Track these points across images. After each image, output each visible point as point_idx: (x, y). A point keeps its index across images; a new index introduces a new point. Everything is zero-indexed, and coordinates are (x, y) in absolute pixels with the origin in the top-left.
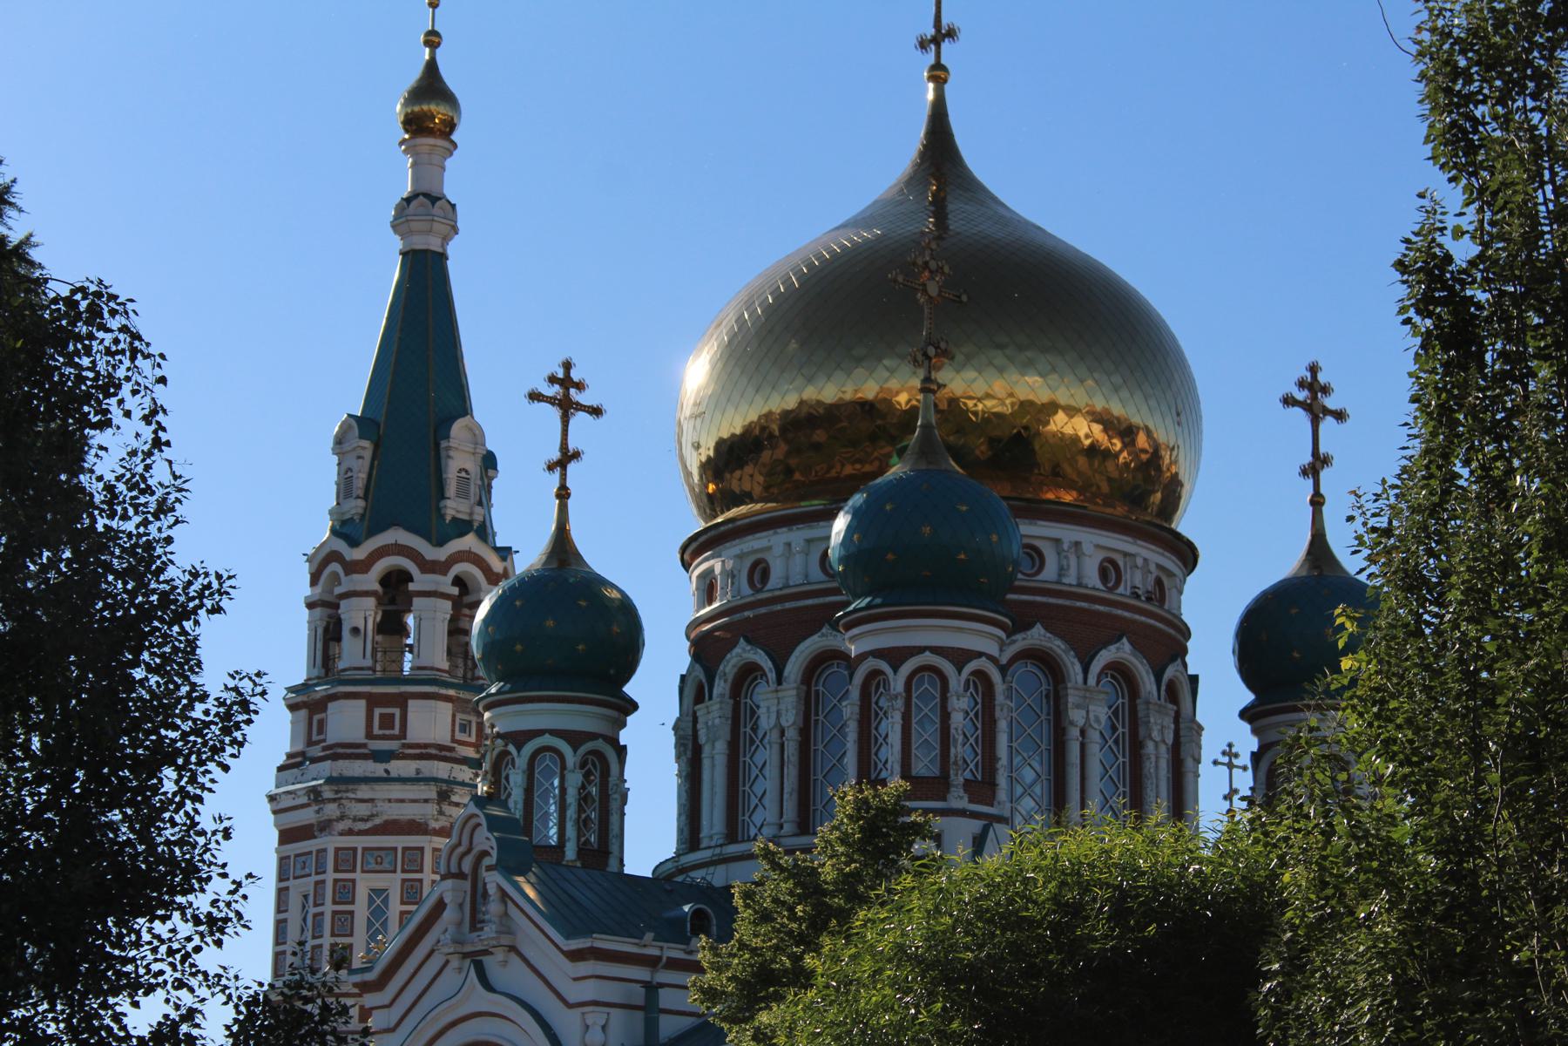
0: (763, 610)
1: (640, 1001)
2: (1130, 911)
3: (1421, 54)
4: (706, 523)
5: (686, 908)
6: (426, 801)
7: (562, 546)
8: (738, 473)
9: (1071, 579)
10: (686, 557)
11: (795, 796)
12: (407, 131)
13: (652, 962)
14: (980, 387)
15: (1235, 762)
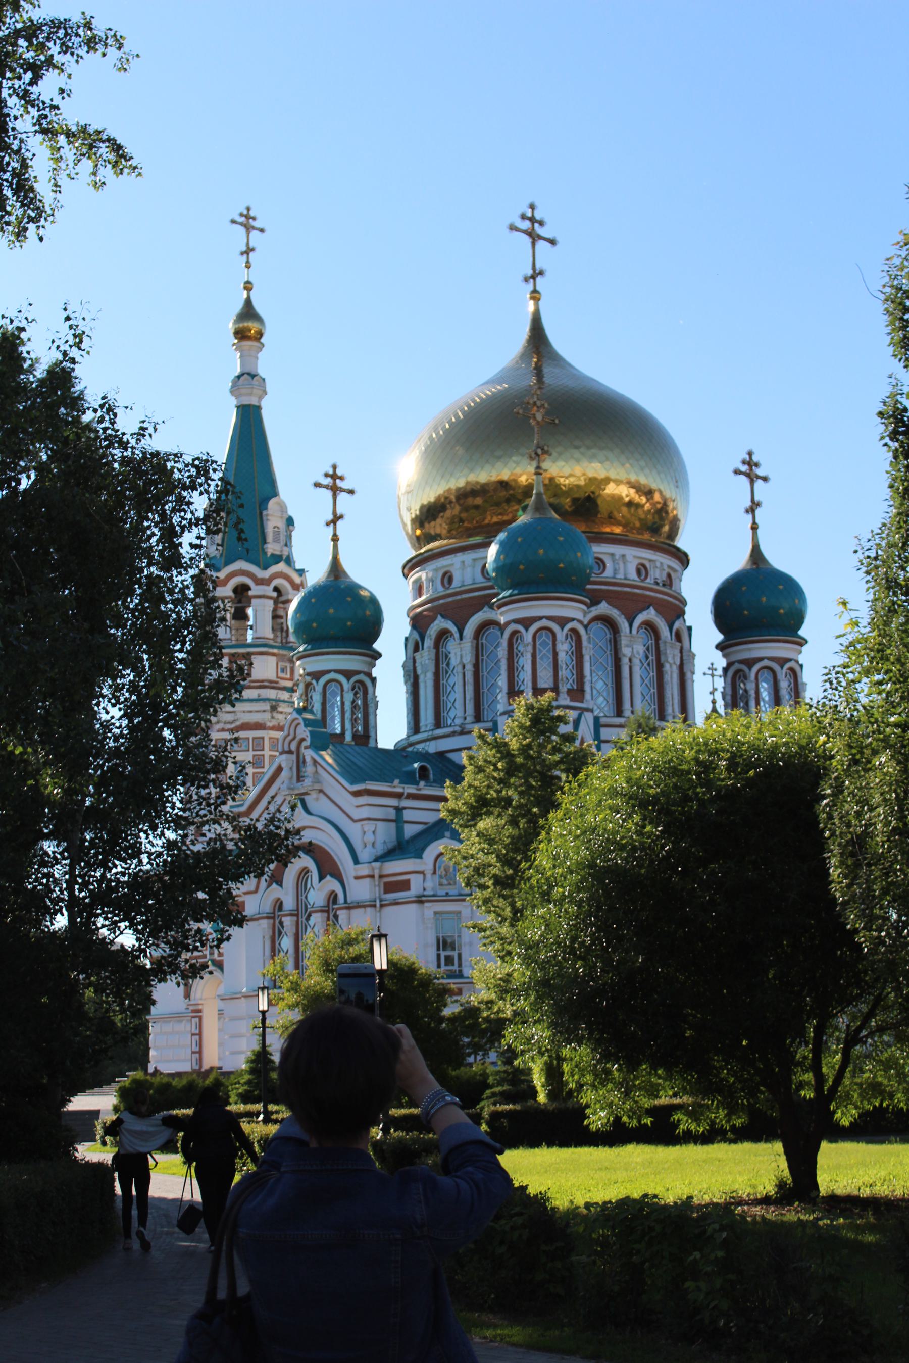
0: (450, 599)
1: (393, 817)
2: (738, 764)
3: (886, 300)
4: (416, 550)
5: (416, 765)
6: (264, 711)
7: (336, 568)
8: (433, 523)
9: (620, 576)
10: (406, 571)
11: (472, 701)
12: (236, 338)
13: (399, 796)
14: (567, 471)
15: (715, 673)
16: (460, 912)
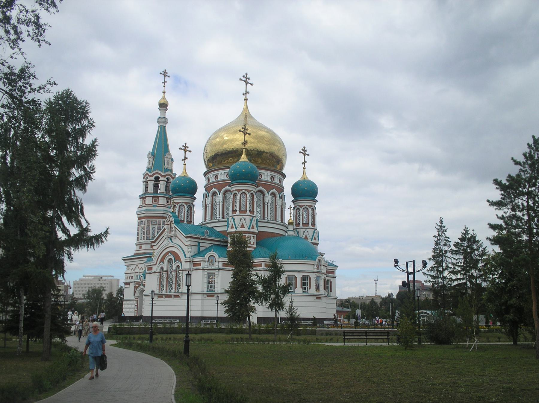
13: (199, 239)
16: (215, 273)
